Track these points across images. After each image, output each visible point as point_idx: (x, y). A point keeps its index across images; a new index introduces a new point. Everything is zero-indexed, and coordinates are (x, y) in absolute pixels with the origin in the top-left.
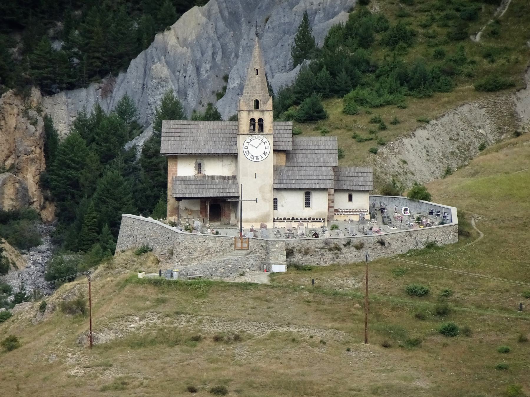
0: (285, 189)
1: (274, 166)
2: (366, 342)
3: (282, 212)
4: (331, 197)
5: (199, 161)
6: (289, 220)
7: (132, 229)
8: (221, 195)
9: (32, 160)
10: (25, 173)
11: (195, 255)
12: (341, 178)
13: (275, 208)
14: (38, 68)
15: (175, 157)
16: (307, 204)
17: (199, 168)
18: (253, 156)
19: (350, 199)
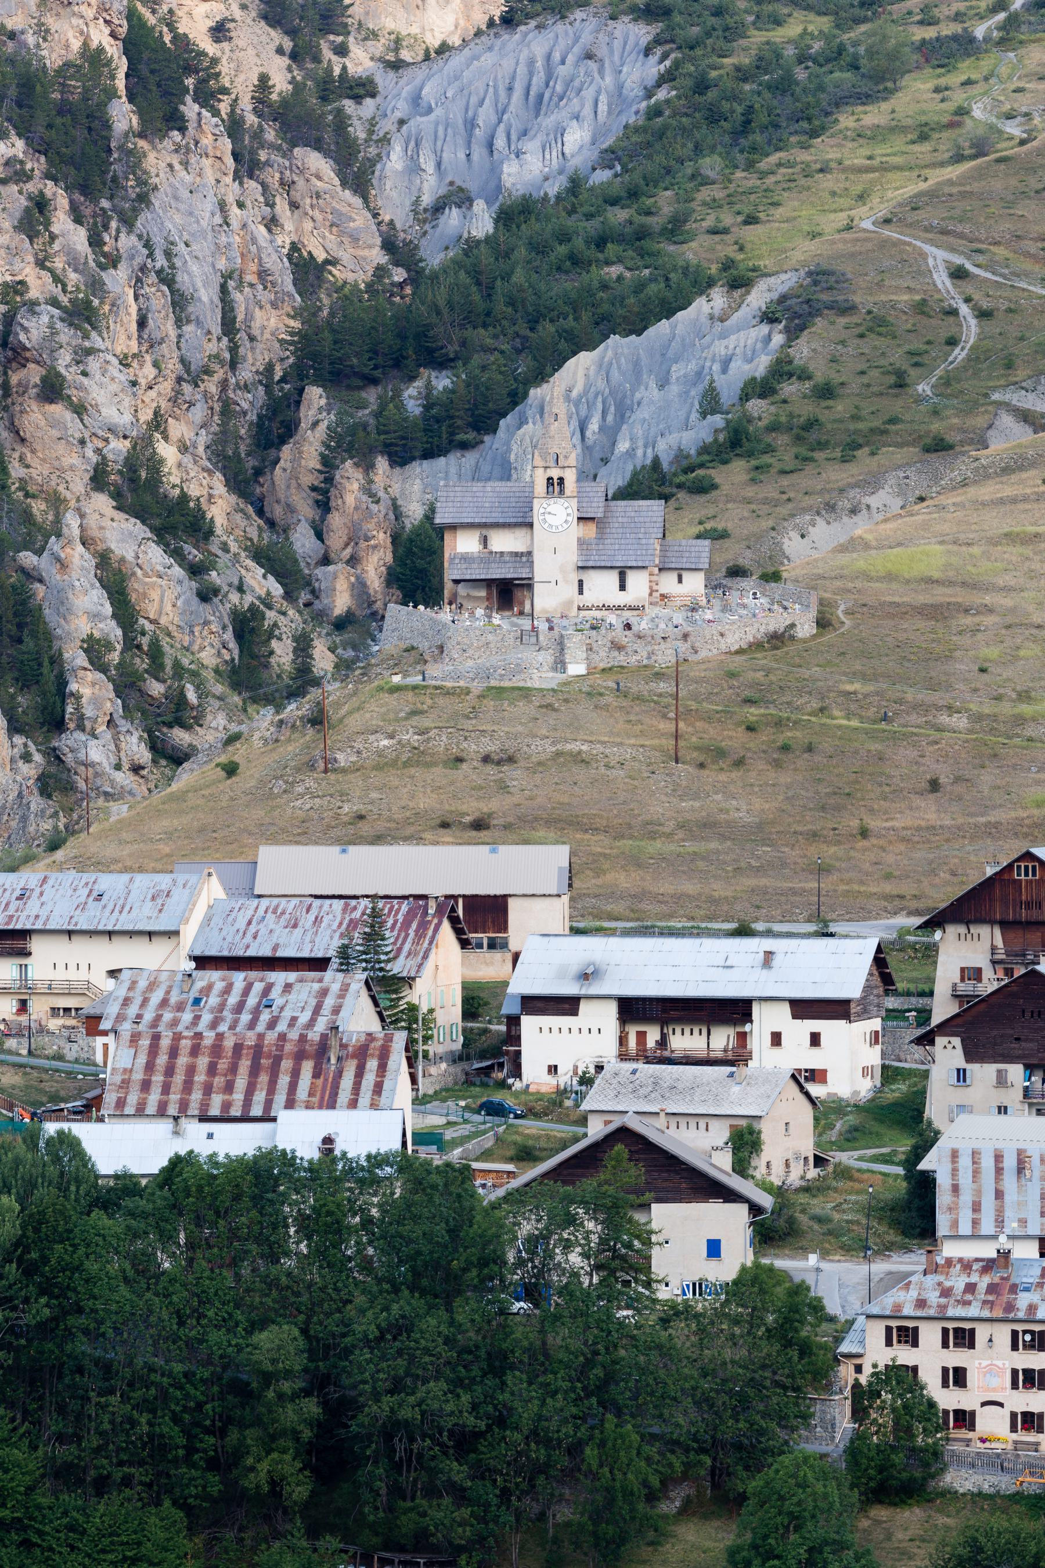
0: (593, 567)
1: (579, 539)
2: (677, 762)
3: (590, 597)
4: (654, 578)
5: (485, 532)
6: (598, 608)
7: (397, 621)
8: (509, 576)
9: (375, 547)
10: (365, 563)
11: (470, 652)
12: (669, 554)
13: (581, 592)
14: (387, 433)
15: (454, 527)
16: (623, 587)
17: (485, 541)
18: (551, 526)
19: (680, 581)
